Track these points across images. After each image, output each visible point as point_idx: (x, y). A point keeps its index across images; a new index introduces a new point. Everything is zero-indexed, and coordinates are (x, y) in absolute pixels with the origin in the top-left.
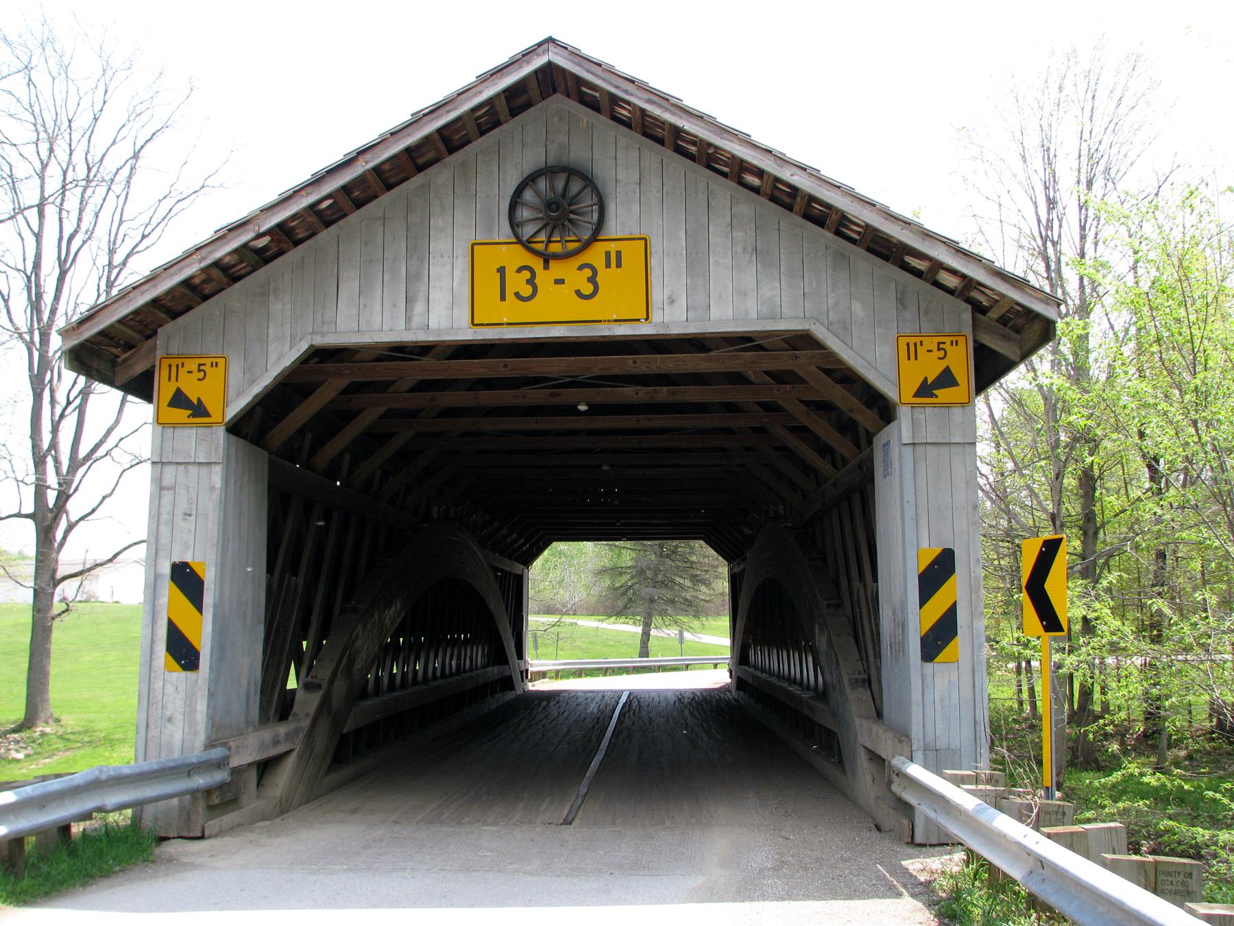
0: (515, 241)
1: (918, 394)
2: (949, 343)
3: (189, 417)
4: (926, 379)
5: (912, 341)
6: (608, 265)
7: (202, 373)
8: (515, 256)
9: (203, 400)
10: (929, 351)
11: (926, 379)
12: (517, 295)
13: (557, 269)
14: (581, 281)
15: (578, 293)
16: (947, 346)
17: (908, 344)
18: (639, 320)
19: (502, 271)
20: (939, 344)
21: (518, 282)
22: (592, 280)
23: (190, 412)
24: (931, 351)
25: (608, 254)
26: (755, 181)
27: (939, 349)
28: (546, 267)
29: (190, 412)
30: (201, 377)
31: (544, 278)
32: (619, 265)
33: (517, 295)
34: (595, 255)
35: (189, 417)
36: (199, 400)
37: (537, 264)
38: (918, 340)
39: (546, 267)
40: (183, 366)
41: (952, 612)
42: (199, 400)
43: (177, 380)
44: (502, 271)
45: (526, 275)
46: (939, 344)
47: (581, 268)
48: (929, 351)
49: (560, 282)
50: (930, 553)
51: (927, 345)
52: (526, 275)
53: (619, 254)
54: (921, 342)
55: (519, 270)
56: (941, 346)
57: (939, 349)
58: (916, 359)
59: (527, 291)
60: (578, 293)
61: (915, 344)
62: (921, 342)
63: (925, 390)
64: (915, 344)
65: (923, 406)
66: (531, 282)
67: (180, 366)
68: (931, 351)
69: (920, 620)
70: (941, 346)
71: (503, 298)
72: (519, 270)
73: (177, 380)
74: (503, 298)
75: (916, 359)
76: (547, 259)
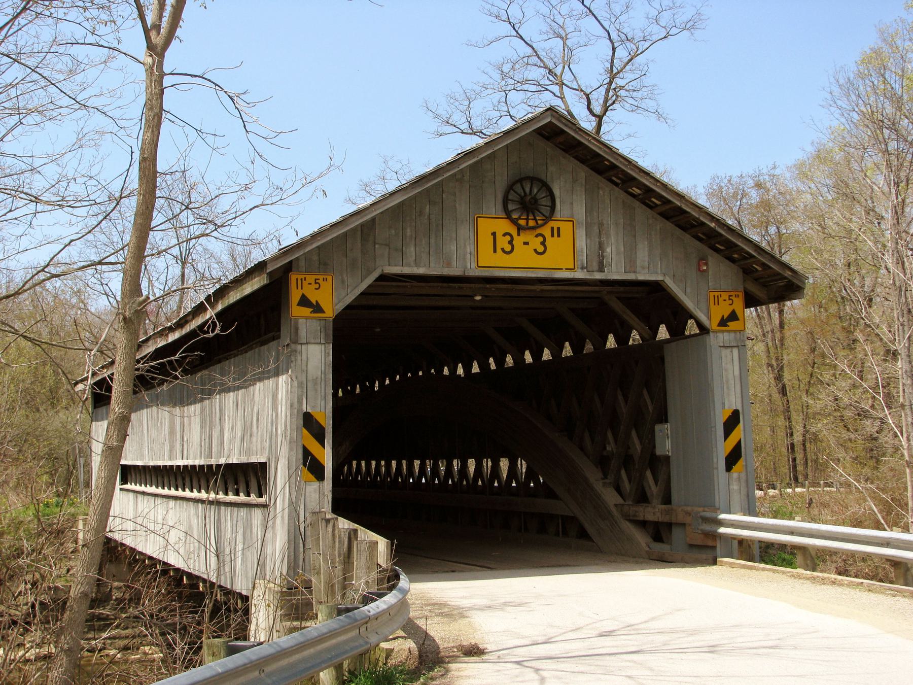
0: (506, 217)
1: (719, 325)
2: (734, 296)
3: (311, 313)
4: (723, 316)
5: (716, 294)
6: (553, 235)
7: (731, 301)
8: (503, 226)
9: (319, 302)
10: (725, 300)
11: (723, 316)
12: (503, 250)
13: (524, 237)
14: (536, 243)
15: (535, 250)
16: (320, 281)
17: (297, 279)
18: (562, 269)
19: (494, 234)
20: (316, 280)
21: (503, 242)
22: (543, 243)
23: (725, 318)
24: (311, 284)
25: (552, 229)
26: (636, 191)
27: (316, 283)
28: (519, 234)
29: (725, 318)
30: (731, 303)
31: (518, 241)
32: (559, 236)
33: (503, 250)
34: (546, 231)
35: (311, 313)
36: (317, 302)
37: (514, 232)
38: (719, 294)
39: (519, 234)
40: (305, 280)
41: (739, 444)
42: (317, 302)
43: (302, 289)
44: (494, 234)
45: (508, 238)
46: (316, 280)
47: (537, 236)
48: (725, 300)
49: (526, 243)
50: (728, 413)
51: (308, 280)
52: (508, 238)
53: (558, 229)
54: (305, 278)
55: (505, 235)
56: (317, 281)
57: (316, 283)
58: (718, 304)
59: (508, 248)
60: (535, 250)
61: (302, 279)
62: (305, 278)
63: (723, 323)
64: (302, 279)
65: (723, 331)
66: (511, 242)
67: (303, 280)
68: (311, 284)
69: (723, 448)
70: (317, 281)
71: (495, 251)
72: (505, 235)
73: (302, 289)
74: (495, 251)
75: (718, 304)
76: (520, 229)
